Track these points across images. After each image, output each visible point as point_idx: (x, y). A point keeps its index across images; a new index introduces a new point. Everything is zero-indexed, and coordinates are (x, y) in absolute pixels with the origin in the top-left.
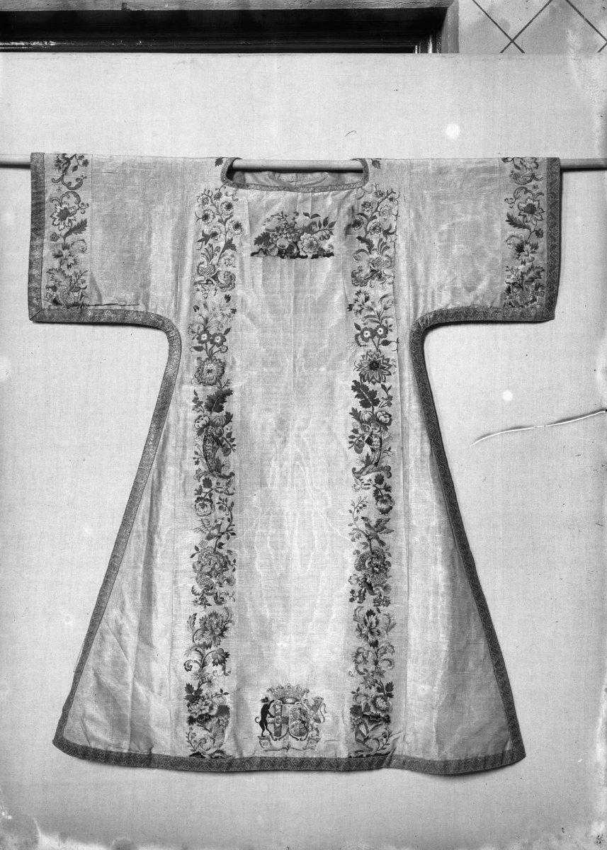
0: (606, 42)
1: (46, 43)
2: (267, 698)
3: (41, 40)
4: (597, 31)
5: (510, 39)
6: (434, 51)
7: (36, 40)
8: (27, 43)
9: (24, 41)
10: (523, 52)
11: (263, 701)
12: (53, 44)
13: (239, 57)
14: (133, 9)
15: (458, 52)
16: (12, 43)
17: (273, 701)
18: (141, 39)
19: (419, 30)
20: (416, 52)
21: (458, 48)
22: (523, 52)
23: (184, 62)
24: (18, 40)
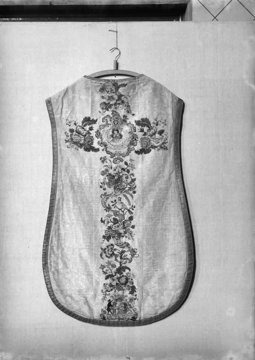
0: (254, 18)
1: (18, 19)
2: (110, 300)
3: (16, 17)
4: (203, 5)
5: (214, 17)
6: (182, 20)
7: (13, 17)
8: (10, 19)
9: (8, 18)
10: (218, 20)
11: (108, 301)
12: (20, 19)
13: (109, 23)
14: (54, 5)
15: (191, 20)
16: (4, 19)
17: (112, 301)
18: (58, 17)
19: (177, 12)
20: (180, 20)
21: (192, 19)
22: (218, 20)
23: (86, 26)
24: (6, 18)
